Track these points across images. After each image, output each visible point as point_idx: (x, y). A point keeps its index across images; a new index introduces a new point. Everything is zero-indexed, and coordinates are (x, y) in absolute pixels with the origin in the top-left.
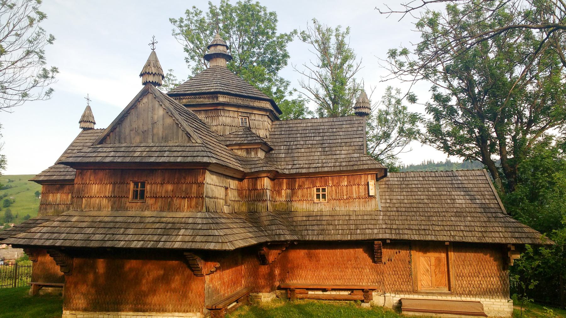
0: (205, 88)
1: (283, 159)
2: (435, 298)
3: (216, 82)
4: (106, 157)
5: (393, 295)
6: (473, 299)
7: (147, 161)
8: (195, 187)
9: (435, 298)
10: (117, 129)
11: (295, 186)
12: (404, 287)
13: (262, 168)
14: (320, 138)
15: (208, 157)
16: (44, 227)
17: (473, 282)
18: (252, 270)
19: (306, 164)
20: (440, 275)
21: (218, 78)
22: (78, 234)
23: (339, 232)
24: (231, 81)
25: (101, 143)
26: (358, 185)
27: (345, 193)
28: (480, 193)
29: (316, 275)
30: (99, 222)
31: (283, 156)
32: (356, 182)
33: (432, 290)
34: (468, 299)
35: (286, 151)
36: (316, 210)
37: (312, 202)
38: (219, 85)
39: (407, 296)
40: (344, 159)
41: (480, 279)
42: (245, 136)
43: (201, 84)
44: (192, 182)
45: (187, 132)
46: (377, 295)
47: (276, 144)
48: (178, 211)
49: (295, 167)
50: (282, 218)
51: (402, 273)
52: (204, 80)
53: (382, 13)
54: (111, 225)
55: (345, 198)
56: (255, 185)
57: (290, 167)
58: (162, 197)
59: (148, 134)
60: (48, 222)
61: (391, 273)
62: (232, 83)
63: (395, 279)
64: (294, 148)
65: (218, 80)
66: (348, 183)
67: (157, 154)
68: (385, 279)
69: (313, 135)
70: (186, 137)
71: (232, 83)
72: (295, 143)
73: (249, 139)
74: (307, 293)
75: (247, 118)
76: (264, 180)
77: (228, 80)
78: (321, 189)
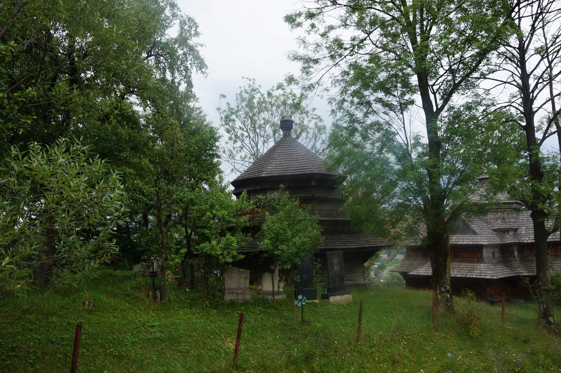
1: (524, 235)
31: (524, 232)
35: (526, 230)
49: (530, 239)
57: (527, 239)
67: (462, 240)
73: (504, 225)
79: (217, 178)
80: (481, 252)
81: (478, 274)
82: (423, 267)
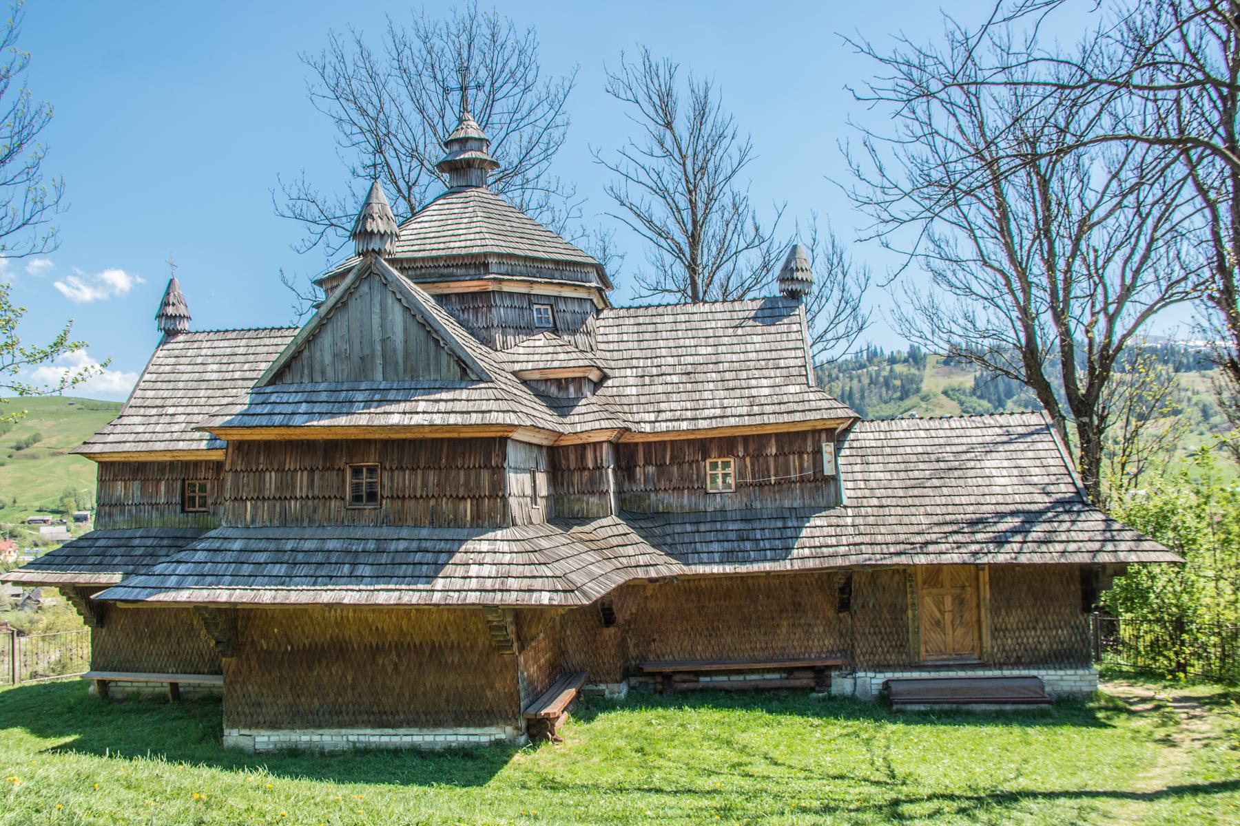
0: (457, 244)
2: (952, 674)
3: (478, 230)
4: (293, 414)
5: (871, 674)
6: (1025, 673)
7: (383, 422)
8: (485, 476)
9: (952, 674)
10: (306, 353)
11: (664, 457)
12: (892, 658)
13: (597, 422)
14: (710, 350)
15: (515, 412)
16: (179, 562)
17: (1025, 640)
18: (582, 638)
19: (687, 410)
20: (963, 630)
21: (479, 219)
22: (256, 576)
23: (766, 555)
24: (507, 223)
25: (271, 383)
26: (801, 454)
27: (772, 472)
28: (1038, 462)
29: (713, 642)
30: (291, 551)
32: (796, 447)
33: (946, 660)
34: (1016, 673)
36: (710, 509)
37: (703, 491)
38: (487, 236)
39: (898, 675)
40: (769, 398)
41: (1038, 633)
42: (551, 350)
43: (445, 233)
44: (480, 467)
45: (459, 358)
46: (839, 676)
47: (613, 364)
48: (452, 525)
49: (663, 416)
50: (642, 528)
51: (888, 630)
52: (450, 222)
53: (859, 99)
54: (319, 557)
55: (773, 482)
56: (582, 461)
58: (415, 496)
59: (373, 362)
60: (183, 553)
61: (867, 631)
62: (510, 229)
63: (875, 643)
64: (655, 373)
65: (481, 224)
66: (777, 450)
68: (856, 644)
69: (693, 342)
70: (456, 367)
71: (510, 229)
72: (656, 362)
74: (698, 681)
75: (549, 307)
76: (601, 449)
77: (501, 222)
78: (720, 463)
79: (703, 584)
80: (499, 472)
81: (489, 584)
82: (182, 555)
